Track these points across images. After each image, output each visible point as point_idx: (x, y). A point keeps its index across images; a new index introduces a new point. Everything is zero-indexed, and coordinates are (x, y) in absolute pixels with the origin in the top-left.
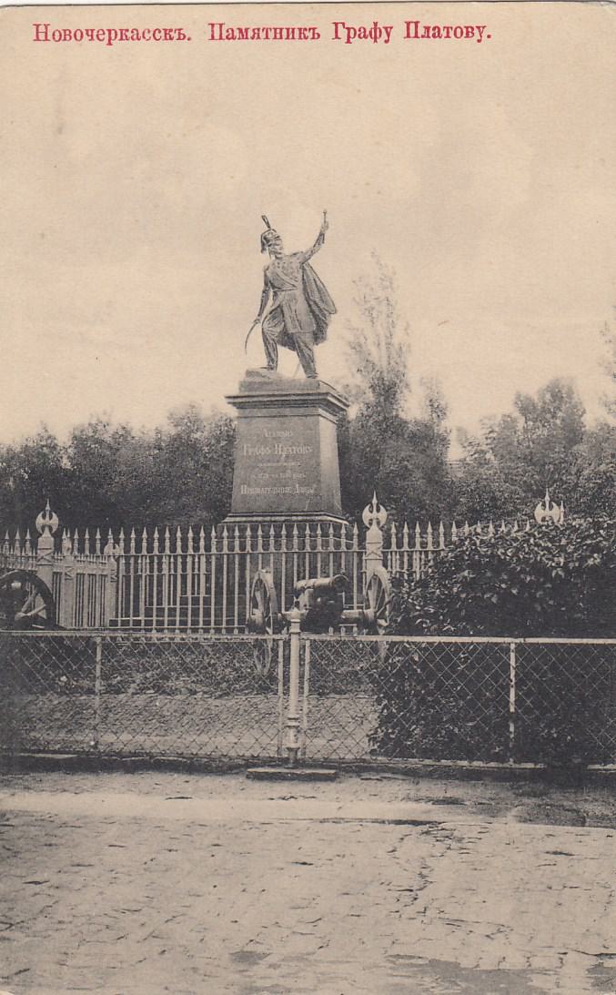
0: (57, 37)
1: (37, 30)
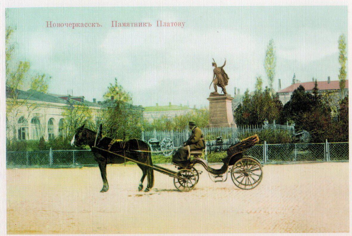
0: (55, 26)
1: (51, 25)
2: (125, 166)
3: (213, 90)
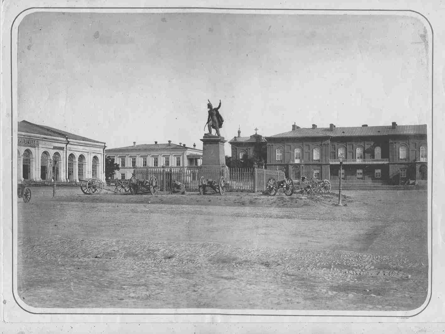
3: (207, 131)
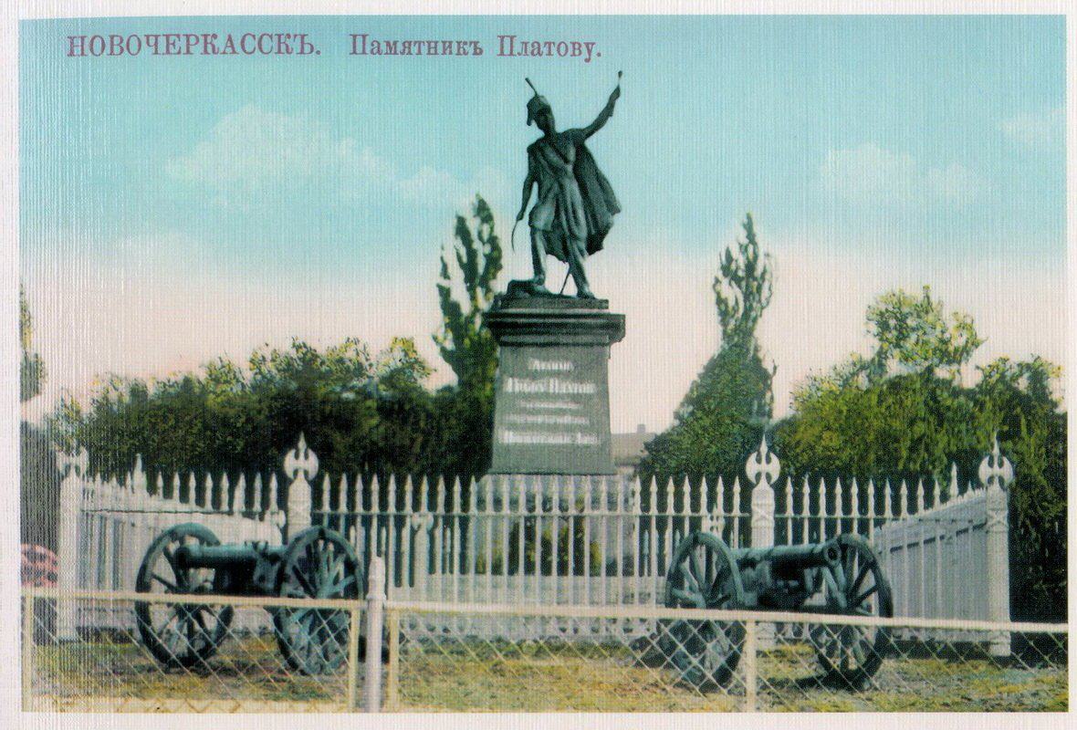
0: (98, 43)
2: (475, 216)
